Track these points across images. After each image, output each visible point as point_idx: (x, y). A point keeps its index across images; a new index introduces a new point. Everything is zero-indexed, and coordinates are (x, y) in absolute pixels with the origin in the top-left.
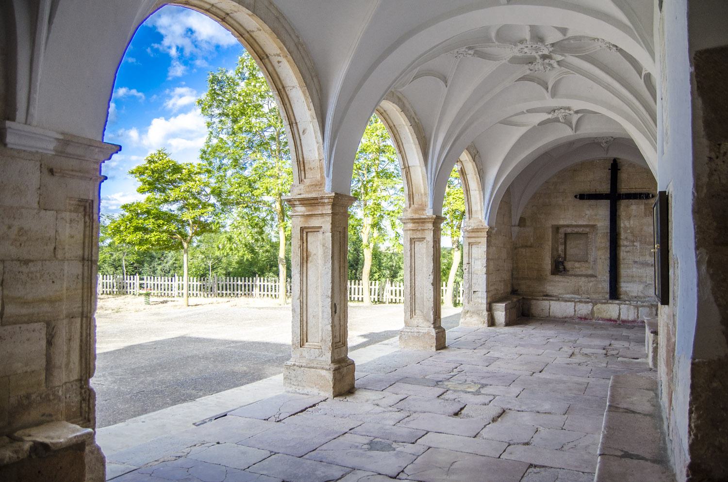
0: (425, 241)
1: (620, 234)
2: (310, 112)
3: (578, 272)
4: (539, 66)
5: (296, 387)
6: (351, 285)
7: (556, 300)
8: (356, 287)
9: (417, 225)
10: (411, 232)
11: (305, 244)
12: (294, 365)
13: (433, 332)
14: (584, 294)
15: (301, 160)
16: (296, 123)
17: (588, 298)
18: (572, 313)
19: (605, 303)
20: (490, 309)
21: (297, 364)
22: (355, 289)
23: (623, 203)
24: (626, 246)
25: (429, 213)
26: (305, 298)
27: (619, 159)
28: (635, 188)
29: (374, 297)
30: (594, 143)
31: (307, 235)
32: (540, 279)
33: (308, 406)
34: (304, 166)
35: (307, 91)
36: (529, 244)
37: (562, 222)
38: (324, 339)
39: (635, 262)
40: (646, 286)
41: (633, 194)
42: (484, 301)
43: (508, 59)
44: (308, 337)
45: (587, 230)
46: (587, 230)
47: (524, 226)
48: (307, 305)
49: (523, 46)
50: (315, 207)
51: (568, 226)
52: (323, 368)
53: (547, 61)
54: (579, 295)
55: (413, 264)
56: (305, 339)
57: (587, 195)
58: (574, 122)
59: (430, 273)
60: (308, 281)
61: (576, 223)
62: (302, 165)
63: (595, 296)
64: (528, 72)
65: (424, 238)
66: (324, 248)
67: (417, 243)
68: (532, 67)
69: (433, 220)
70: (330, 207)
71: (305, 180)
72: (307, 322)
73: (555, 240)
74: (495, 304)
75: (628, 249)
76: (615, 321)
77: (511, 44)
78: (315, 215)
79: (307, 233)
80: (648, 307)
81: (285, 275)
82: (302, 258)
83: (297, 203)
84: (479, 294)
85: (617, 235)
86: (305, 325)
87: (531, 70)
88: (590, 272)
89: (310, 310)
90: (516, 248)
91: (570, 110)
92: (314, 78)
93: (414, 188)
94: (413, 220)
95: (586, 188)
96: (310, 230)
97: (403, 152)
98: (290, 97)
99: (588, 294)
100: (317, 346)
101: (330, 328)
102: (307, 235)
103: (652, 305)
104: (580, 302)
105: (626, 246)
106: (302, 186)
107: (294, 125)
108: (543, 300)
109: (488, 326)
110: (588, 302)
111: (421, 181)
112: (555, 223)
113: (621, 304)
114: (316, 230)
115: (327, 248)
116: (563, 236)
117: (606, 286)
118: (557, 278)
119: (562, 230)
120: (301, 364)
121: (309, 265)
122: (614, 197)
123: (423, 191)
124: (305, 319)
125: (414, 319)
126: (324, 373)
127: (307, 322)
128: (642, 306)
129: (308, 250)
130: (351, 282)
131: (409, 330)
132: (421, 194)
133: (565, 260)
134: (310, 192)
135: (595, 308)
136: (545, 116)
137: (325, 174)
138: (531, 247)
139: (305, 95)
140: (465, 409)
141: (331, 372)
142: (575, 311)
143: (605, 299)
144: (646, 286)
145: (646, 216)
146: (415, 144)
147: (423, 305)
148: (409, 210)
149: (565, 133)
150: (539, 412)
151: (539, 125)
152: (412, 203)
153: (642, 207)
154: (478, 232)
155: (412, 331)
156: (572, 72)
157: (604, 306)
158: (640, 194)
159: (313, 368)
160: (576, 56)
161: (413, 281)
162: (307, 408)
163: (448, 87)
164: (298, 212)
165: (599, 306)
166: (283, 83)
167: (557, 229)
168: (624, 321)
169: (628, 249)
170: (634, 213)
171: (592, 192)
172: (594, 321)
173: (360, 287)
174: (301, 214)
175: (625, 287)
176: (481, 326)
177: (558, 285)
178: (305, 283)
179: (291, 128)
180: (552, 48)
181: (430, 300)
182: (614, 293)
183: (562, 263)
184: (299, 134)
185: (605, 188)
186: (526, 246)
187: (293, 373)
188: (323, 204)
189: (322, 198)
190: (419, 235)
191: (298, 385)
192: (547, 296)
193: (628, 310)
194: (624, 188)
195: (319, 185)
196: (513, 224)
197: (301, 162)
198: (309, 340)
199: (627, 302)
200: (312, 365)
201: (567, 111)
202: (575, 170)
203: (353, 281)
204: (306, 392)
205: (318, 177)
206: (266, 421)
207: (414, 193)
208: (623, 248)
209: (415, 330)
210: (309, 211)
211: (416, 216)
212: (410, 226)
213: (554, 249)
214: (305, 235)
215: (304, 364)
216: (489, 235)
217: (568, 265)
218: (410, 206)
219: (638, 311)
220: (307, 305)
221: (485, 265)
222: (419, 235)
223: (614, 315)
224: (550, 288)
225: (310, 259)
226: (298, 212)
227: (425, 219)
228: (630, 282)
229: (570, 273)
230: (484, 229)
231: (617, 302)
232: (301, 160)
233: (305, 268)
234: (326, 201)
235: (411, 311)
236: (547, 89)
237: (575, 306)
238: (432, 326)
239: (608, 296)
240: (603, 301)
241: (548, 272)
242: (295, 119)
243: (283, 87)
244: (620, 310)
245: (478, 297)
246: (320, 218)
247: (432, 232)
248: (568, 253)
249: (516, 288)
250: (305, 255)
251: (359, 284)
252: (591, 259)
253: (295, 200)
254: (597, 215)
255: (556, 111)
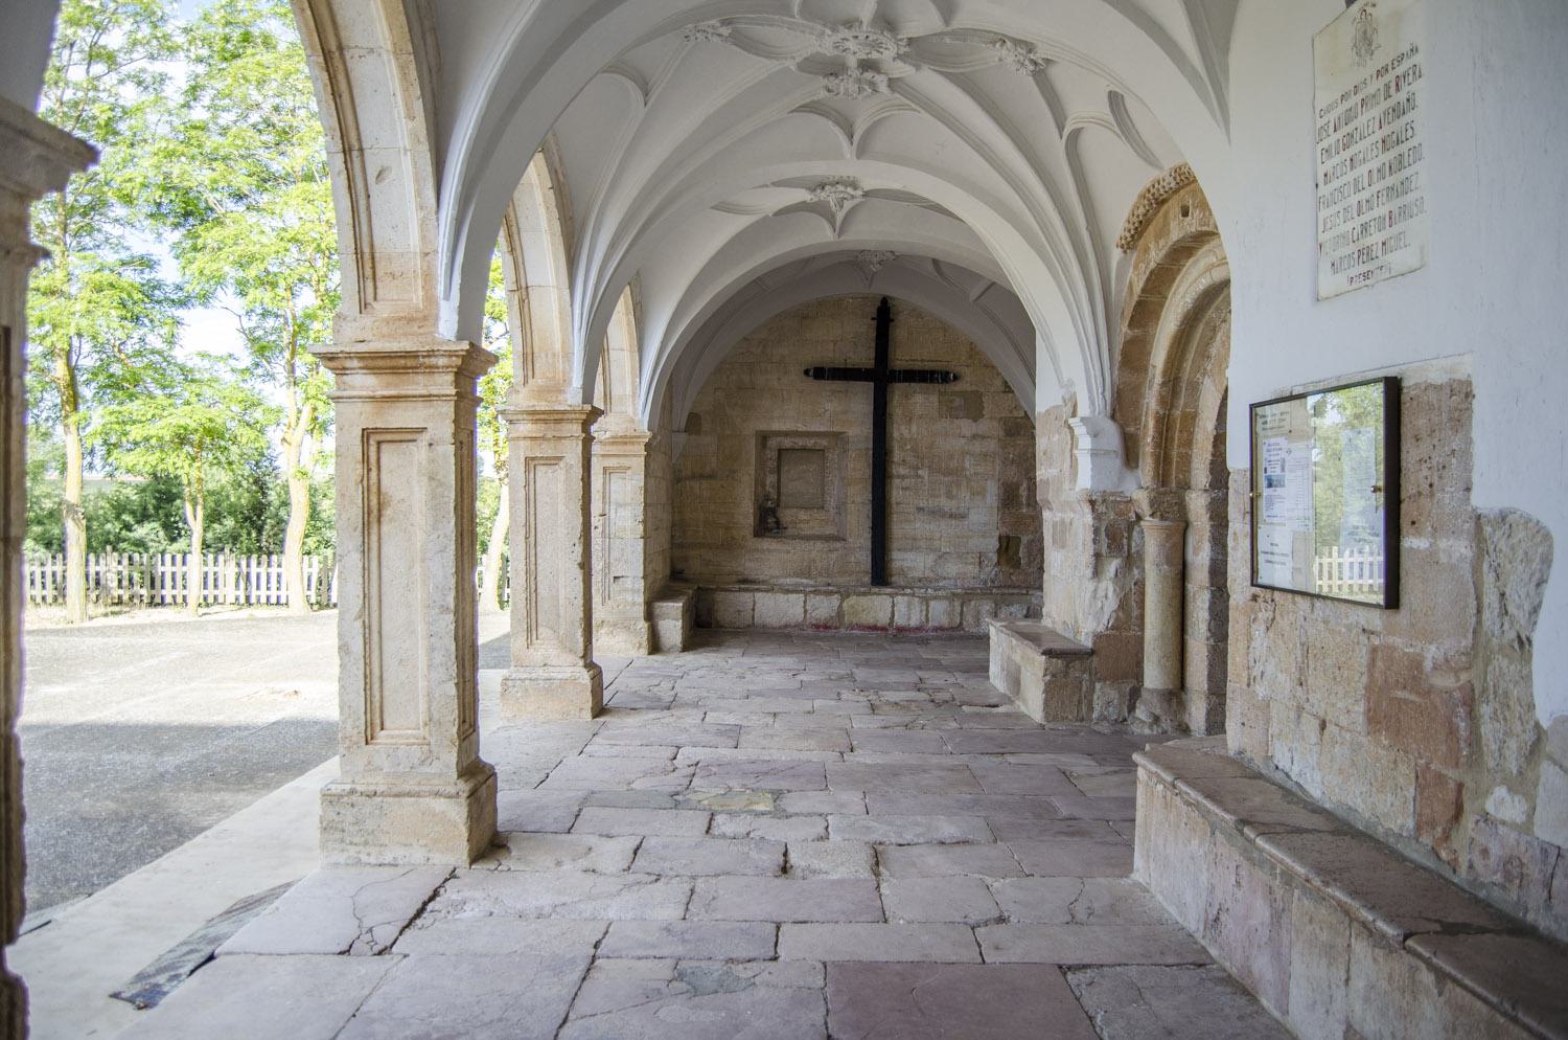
0: (562, 464)
1: (891, 452)
2: (411, 124)
3: (807, 530)
4: (847, 85)
5: (361, 848)
6: (248, 565)
7: (767, 591)
8: (263, 570)
9: (543, 426)
10: (528, 442)
11: (374, 474)
12: (352, 792)
13: (585, 677)
14: (821, 575)
15: (366, 250)
16: (361, 150)
17: (829, 585)
18: (800, 618)
19: (864, 594)
20: (650, 616)
21: (359, 788)
22: (258, 576)
23: (898, 391)
24: (903, 477)
25: (572, 398)
26: (375, 615)
27: (892, 298)
28: (922, 360)
29: (258, 593)
30: (853, 262)
31: (379, 448)
32: (730, 546)
33: (426, 898)
34: (373, 268)
35: (413, 66)
36: (708, 470)
37: (776, 426)
38: (436, 717)
39: (920, 509)
40: (940, 557)
41: (920, 372)
42: (640, 599)
43: (798, 60)
44: (385, 717)
45: (824, 442)
46: (824, 442)
47: (698, 433)
48: (380, 633)
49: (847, 34)
50: (405, 377)
51: (786, 434)
52: (437, 794)
53: (868, 75)
54: (809, 577)
55: (532, 519)
56: (378, 721)
57: (829, 369)
58: (840, 216)
59: (577, 541)
60: (384, 570)
61: (804, 429)
62: (368, 265)
63: (841, 580)
64: (823, 94)
65: (560, 458)
66: (434, 484)
67: (541, 470)
68: (832, 82)
69: (584, 417)
70: (450, 378)
71: (374, 304)
72: (381, 677)
73: (761, 463)
74: (660, 604)
75: (906, 483)
76: (883, 629)
77: (825, 25)
78: (406, 397)
79: (379, 443)
80: (945, 598)
81: (84, 547)
82: (367, 512)
83: (356, 363)
84: (628, 583)
85: (886, 454)
86: (376, 686)
87: (829, 91)
88: (829, 530)
89: (389, 647)
90: (679, 481)
91: (855, 189)
92: (428, 34)
93: (536, 338)
94: (535, 415)
95: (829, 356)
96: (389, 437)
97: (519, 251)
98: (352, 75)
99: (829, 576)
100: (414, 737)
101: (453, 691)
102: (379, 448)
103: (954, 594)
104: (816, 592)
105: (903, 477)
106: (367, 320)
107: (355, 154)
108: (740, 590)
109: (650, 654)
110: (831, 593)
111: (557, 323)
112: (763, 427)
113: (897, 594)
114: (407, 435)
115: (441, 484)
116: (774, 455)
117: (862, 558)
118: (766, 544)
119: (773, 443)
120: (372, 788)
121: (385, 528)
122: (882, 376)
123: (558, 346)
124: (376, 671)
125: (536, 650)
126: (440, 805)
127: (381, 677)
128: (935, 598)
129: (383, 490)
130: (249, 558)
131: (525, 676)
132: (554, 355)
133: (778, 505)
134: (391, 336)
135: (845, 604)
136: (801, 195)
137: (441, 289)
138: (711, 476)
139: (404, 76)
140: (790, 851)
141: (463, 801)
142: (806, 611)
143: (863, 585)
144: (940, 557)
145: (941, 417)
146: (553, 235)
147: (558, 615)
148: (524, 391)
149: (818, 236)
150: (943, 843)
151: (775, 214)
152: (530, 373)
153: (934, 398)
154: (626, 443)
155: (534, 676)
156: (913, 106)
157: (863, 600)
158: (933, 372)
159: (409, 794)
160: (941, 73)
161: (533, 559)
162: (425, 904)
163: (649, 104)
164: (353, 388)
165: (853, 600)
166: (343, 34)
167: (763, 438)
168: (900, 629)
169: (906, 483)
170: (918, 410)
171: (839, 363)
172: (843, 630)
173: (274, 571)
174: (364, 393)
175: (907, 561)
176: (633, 653)
177: (772, 558)
178: (374, 576)
179: (345, 162)
180: (907, 49)
181: (576, 602)
182: (881, 574)
183: (773, 512)
184: (365, 180)
185: (864, 357)
186: (702, 476)
187: (349, 815)
188: (432, 369)
189: (431, 354)
190: (547, 450)
191: (366, 843)
192: (745, 581)
193: (909, 606)
194: (901, 358)
195: (428, 317)
196: (675, 428)
197: (367, 256)
198: (387, 724)
199: (909, 591)
200: (407, 788)
201: (849, 189)
202: (804, 316)
203: (255, 556)
204: (388, 858)
205: (417, 298)
206: (345, 957)
207: (536, 350)
208: (896, 482)
209: (541, 673)
210: (388, 386)
211: (542, 406)
212: (526, 428)
213: (759, 483)
214: (373, 449)
215: (380, 788)
216: (648, 446)
217: (786, 516)
218: (525, 382)
219: (928, 606)
220: (380, 633)
221: (641, 518)
222: (547, 450)
223: (883, 618)
224: (750, 566)
225: (388, 512)
226: (353, 388)
227: (564, 412)
228: (911, 550)
229: (790, 531)
230: (639, 437)
231: (889, 590)
232: (366, 250)
233: (374, 538)
234: (442, 361)
235: (529, 630)
236: (851, 137)
237: (805, 602)
238: (581, 663)
239: (867, 579)
240: (862, 589)
241: (748, 532)
242: (359, 139)
243: (341, 48)
244: (893, 607)
245: (626, 590)
246: (420, 405)
247: (580, 443)
248: (783, 490)
249: (679, 566)
250: (374, 502)
251: (269, 565)
252: (831, 503)
253: (349, 356)
254: (850, 411)
255: (827, 187)
